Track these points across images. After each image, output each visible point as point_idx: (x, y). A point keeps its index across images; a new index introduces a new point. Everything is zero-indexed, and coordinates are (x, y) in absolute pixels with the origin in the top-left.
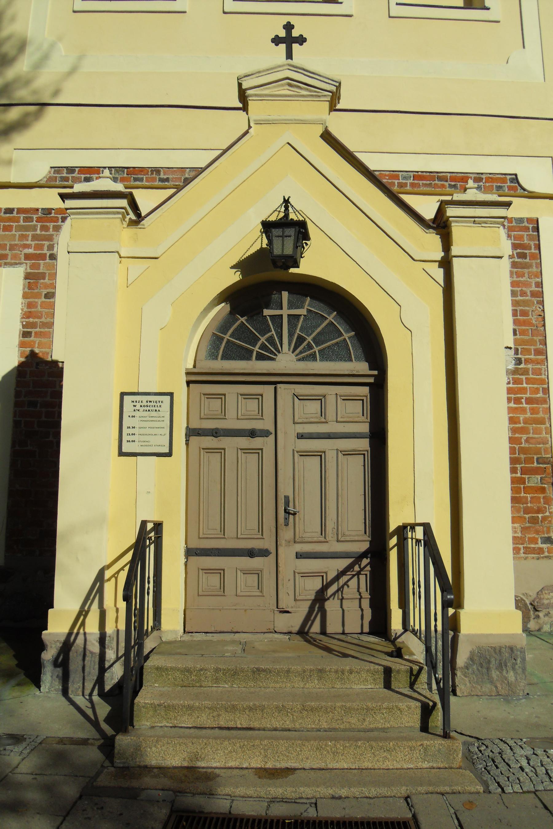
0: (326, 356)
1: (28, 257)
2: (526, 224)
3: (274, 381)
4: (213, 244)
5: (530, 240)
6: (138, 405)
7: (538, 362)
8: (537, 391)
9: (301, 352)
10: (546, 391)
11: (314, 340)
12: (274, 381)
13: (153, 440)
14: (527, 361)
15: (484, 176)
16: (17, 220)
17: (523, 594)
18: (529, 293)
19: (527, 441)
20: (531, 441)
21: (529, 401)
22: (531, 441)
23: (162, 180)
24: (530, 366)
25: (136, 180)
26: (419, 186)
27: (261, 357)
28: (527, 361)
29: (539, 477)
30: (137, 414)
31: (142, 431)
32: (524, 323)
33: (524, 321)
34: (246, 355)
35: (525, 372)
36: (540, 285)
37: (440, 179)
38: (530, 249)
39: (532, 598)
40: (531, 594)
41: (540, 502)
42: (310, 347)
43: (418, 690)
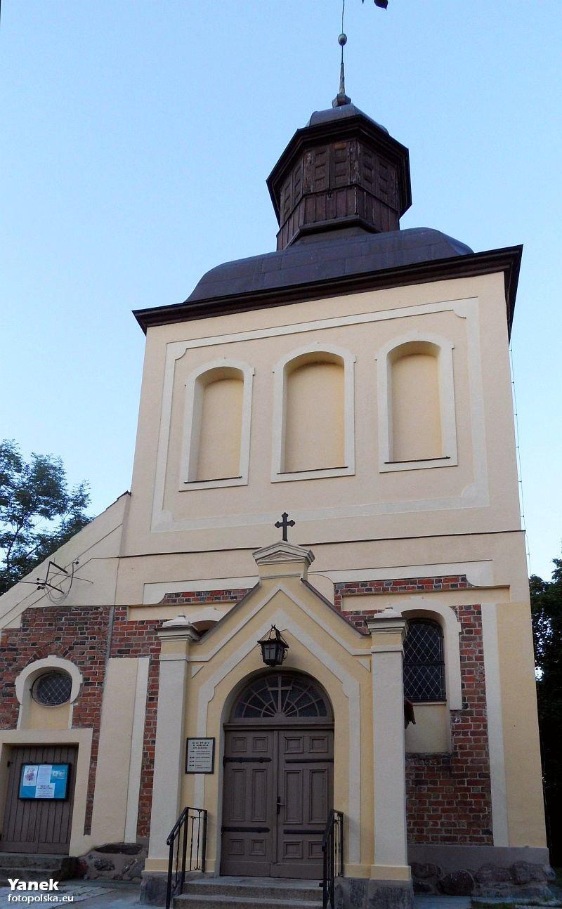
0: (304, 712)
1: (152, 651)
2: (472, 609)
3: (271, 729)
4: (236, 656)
5: (475, 620)
6: (196, 745)
7: (479, 706)
8: (479, 727)
9: (289, 712)
10: (485, 726)
11: (262, 708)
12: (271, 729)
13: (204, 765)
14: (472, 706)
15: (442, 579)
16: (146, 628)
17: (468, 870)
18: (474, 658)
19: (472, 761)
20: (476, 762)
21: (473, 734)
22: (476, 762)
23: (232, 598)
24: (474, 709)
25: (216, 598)
26: (396, 589)
27: (265, 715)
28: (472, 706)
29: (480, 787)
30: (195, 750)
31: (198, 760)
32: (471, 679)
33: (470, 678)
34: (257, 714)
35: (471, 713)
36: (481, 652)
37: (412, 583)
38: (475, 627)
39: (475, 873)
40: (474, 870)
41: (481, 805)
42: (293, 708)
43: (236, 825)
